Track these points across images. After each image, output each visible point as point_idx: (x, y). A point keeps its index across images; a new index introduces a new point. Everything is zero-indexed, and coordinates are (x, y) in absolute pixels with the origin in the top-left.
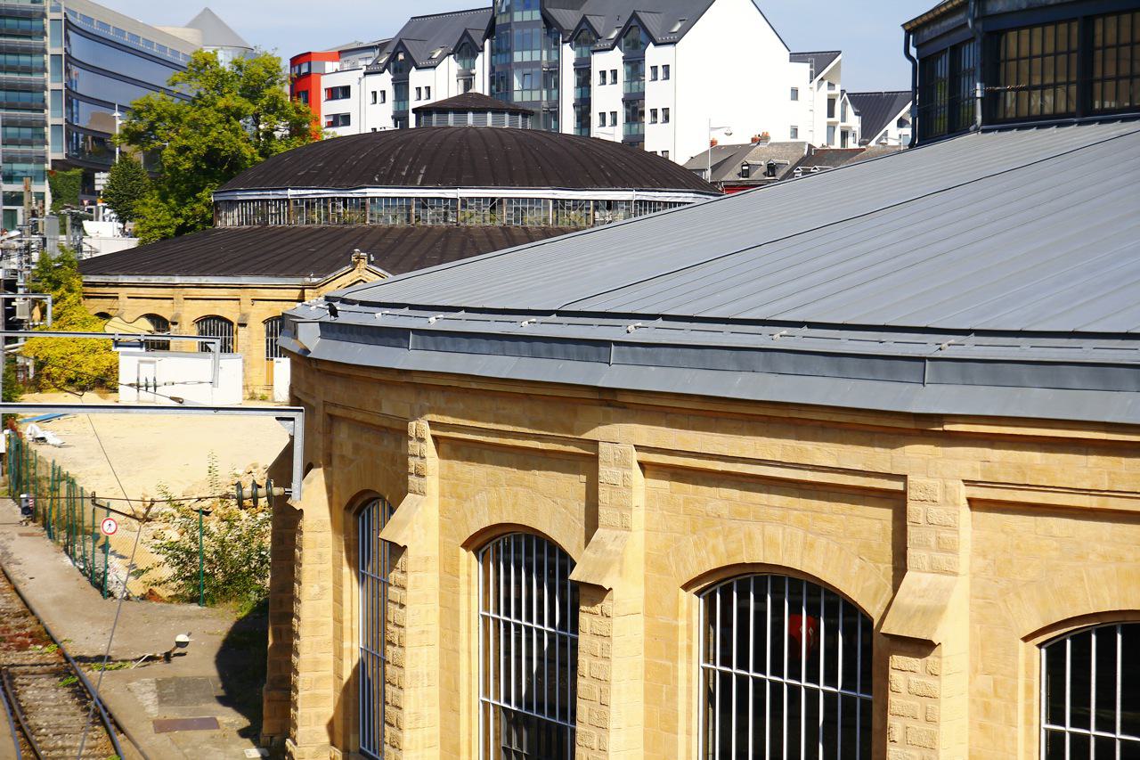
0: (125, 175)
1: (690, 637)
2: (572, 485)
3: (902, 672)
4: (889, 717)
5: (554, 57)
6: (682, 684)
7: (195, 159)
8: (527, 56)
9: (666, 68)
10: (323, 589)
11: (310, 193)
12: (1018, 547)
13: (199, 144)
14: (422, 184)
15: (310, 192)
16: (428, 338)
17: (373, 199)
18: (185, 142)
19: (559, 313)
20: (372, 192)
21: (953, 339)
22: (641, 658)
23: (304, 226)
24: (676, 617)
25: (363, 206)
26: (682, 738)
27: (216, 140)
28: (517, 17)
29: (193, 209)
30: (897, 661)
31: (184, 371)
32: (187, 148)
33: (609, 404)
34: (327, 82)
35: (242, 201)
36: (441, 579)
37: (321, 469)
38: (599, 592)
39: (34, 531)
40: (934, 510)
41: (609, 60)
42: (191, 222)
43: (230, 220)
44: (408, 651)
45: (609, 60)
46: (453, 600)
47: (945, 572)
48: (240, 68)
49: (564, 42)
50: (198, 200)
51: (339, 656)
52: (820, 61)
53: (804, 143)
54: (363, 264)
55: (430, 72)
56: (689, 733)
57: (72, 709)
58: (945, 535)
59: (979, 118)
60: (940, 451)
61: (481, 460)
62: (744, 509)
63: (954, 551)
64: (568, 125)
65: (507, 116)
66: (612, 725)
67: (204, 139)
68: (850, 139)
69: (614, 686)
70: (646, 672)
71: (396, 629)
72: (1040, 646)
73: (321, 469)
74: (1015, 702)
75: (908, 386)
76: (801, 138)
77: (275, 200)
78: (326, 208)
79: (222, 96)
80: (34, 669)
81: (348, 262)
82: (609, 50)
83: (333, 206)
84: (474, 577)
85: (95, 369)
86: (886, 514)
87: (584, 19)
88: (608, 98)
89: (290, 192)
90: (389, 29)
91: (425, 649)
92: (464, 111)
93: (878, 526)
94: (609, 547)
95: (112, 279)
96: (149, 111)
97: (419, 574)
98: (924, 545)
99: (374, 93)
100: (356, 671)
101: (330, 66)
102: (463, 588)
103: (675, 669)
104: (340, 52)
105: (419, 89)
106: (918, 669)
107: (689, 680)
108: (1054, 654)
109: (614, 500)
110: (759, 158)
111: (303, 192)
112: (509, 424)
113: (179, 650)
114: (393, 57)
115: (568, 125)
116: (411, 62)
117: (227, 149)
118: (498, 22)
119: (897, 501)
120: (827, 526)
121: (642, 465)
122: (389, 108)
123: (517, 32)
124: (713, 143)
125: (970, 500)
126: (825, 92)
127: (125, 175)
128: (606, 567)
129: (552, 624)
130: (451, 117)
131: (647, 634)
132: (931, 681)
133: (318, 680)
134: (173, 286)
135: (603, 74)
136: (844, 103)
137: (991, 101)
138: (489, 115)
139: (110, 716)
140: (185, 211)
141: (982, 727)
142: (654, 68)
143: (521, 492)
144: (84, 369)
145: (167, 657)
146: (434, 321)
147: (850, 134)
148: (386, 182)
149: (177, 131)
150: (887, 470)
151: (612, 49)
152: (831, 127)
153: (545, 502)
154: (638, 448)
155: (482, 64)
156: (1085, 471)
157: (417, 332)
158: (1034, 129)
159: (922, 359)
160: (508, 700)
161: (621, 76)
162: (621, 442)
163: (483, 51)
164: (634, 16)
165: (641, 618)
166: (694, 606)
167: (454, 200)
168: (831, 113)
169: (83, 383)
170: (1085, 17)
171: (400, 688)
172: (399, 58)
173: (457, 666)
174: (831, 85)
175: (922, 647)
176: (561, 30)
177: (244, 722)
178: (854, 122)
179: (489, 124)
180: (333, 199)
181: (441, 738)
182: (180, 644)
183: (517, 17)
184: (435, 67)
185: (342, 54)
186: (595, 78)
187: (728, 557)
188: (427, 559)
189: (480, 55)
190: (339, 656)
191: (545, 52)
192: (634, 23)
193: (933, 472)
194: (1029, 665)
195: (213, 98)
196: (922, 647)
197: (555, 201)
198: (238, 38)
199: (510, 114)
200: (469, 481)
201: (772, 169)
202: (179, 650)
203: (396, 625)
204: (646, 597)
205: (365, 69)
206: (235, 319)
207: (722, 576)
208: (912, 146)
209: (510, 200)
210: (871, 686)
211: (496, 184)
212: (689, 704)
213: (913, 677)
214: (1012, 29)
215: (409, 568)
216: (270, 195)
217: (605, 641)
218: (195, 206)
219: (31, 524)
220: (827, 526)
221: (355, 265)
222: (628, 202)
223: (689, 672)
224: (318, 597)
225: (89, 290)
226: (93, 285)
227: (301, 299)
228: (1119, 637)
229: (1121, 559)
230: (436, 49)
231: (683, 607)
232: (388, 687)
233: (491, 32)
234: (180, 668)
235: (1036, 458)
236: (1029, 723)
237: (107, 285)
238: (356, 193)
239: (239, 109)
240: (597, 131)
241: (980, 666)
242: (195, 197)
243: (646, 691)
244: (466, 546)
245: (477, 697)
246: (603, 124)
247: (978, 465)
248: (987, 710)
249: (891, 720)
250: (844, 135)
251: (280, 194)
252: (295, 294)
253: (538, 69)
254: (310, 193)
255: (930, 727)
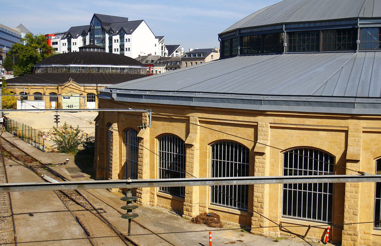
0: (8, 61)
1: (209, 154)
2: (183, 126)
3: (258, 159)
4: (255, 167)
5: (104, 37)
6: (208, 163)
7: (27, 58)
8: (98, 36)
9: (129, 39)
10: (117, 147)
11: (58, 66)
12: (280, 135)
13: (28, 55)
14: (83, 64)
15: (58, 65)
16: (147, 96)
17: (72, 67)
18: (25, 54)
19: (177, 91)
20: (71, 65)
21: (266, 96)
22: (199, 158)
23: (56, 73)
24: (207, 150)
25: (70, 68)
26: (207, 173)
27: (32, 54)
28: (96, 27)
29: (26, 69)
30: (256, 157)
31: (29, 104)
32: (25, 55)
33: (192, 109)
34: (52, 41)
35: (42, 67)
36: (150, 144)
37: (117, 123)
38: (191, 146)
39: (17, 138)
40: (263, 128)
41: (117, 37)
42: (26, 72)
43: (39, 71)
44: (144, 159)
45: (117, 37)
46: (153, 148)
47: (266, 140)
48: (36, 38)
49: (106, 33)
50: (27, 67)
51: (121, 161)
52: (160, 38)
53: (159, 56)
54: (71, 81)
55: (76, 39)
56: (209, 172)
57: (50, 174)
58: (266, 133)
59: (239, 53)
60: (265, 117)
61: (160, 121)
62: (222, 129)
63: (268, 136)
64: (107, 51)
65: (100, 49)
66: (194, 171)
67: (29, 53)
68: (166, 55)
69: (194, 164)
70: (200, 161)
71: (141, 155)
72: (283, 153)
73: (117, 123)
74: (279, 164)
75: (258, 105)
76: (157, 55)
77: (49, 67)
78: (61, 69)
79: (33, 44)
80: (36, 167)
81: (68, 81)
82: (116, 35)
83: (63, 68)
84: (158, 144)
85: (10, 104)
86: (252, 130)
87: (111, 28)
88: (116, 46)
89: (53, 65)
90: (66, 30)
91: (147, 158)
92: (90, 48)
93: (251, 132)
94: (193, 137)
95: (14, 84)
96: (16, 47)
97: (146, 143)
98: (261, 135)
99: (63, 44)
100: (125, 164)
101: (53, 37)
102: (155, 146)
103: (206, 160)
104: (55, 34)
105: (73, 43)
106: (261, 158)
107: (209, 162)
108: (286, 155)
109: (193, 128)
110: (149, 59)
111: (56, 65)
112: (168, 113)
113: (67, 162)
114: (67, 36)
115: (107, 51)
116: (71, 37)
117: (34, 56)
118: (91, 28)
119: (256, 127)
120: (240, 132)
121: (199, 121)
122: (67, 47)
123: (96, 31)
124: (139, 55)
125: (270, 126)
126: (161, 45)
127: (8, 61)
128: (193, 141)
129: (176, 152)
130: (87, 49)
131: (200, 153)
132: (264, 160)
133: (116, 166)
134: (28, 86)
135: (115, 40)
136: (165, 47)
137: (241, 50)
138: (96, 49)
139: (60, 175)
140: (25, 69)
141: (272, 169)
142: (126, 39)
143: (170, 126)
144: (8, 104)
145: (65, 164)
146: (148, 93)
147: (166, 54)
148: (74, 63)
149: (23, 52)
150: (254, 121)
151: (117, 35)
152: (162, 52)
153: (177, 129)
154: (199, 118)
155: (88, 38)
156: (294, 121)
157: (144, 95)
158: (265, 55)
159: (261, 100)
160: (165, 168)
161: (119, 41)
162: (195, 117)
163: (88, 35)
164: (122, 28)
165: (199, 151)
166: (210, 148)
167: (90, 67)
168: (162, 50)
169: (8, 107)
170: (263, 34)
171: (142, 166)
172: (69, 35)
173: (154, 162)
174: (162, 43)
175: (262, 154)
176: (105, 31)
177: (90, 176)
178: (167, 51)
179: (96, 51)
180: (63, 67)
181: (150, 176)
182: (67, 161)
183: (96, 27)
184: (77, 38)
185: (55, 35)
186: (113, 41)
187: (218, 138)
188: (147, 140)
189: (87, 36)
190: (121, 161)
191: (102, 35)
192: (122, 29)
193: (263, 122)
194: (281, 157)
195: (31, 44)
196: (262, 154)
197: (112, 68)
198: (28, 31)
199: (100, 49)
200: (157, 125)
201: (152, 61)
202: (67, 162)
203: (141, 154)
204: (200, 146)
205: (61, 38)
206: (42, 93)
207: (217, 142)
208: (220, 59)
209: (102, 67)
210: (249, 162)
211: (99, 64)
212: (209, 167)
213: (260, 160)
214: (246, 36)
215: (144, 142)
216: (48, 66)
217: (192, 155)
218: (27, 68)
219: (16, 137)
220: (240, 132)
221: (69, 81)
222: (127, 68)
223: (209, 160)
224: (116, 149)
225: (8, 86)
226: (9, 85)
227: (58, 89)
228: (299, 151)
229: (300, 137)
230: (77, 34)
231: (208, 148)
232: (139, 166)
233: (90, 31)
234: (68, 165)
235: (284, 118)
236: (281, 167)
237: (12, 85)
238: (68, 66)
239: (36, 47)
240: (114, 52)
241: (272, 157)
242: (27, 66)
243: (200, 165)
244: (156, 138)
245: (158, 167)
246: (115, 51)
247: (272, 120)
248: (273, 165)
249: (255, 168)
250: (165, 54)
251: (51, 66)
252: (56, 88)
253: (100, 39)
254: (58, 66)
255: (263, 169)
